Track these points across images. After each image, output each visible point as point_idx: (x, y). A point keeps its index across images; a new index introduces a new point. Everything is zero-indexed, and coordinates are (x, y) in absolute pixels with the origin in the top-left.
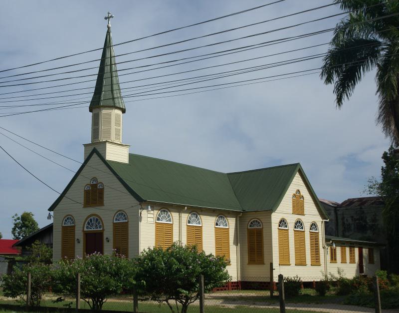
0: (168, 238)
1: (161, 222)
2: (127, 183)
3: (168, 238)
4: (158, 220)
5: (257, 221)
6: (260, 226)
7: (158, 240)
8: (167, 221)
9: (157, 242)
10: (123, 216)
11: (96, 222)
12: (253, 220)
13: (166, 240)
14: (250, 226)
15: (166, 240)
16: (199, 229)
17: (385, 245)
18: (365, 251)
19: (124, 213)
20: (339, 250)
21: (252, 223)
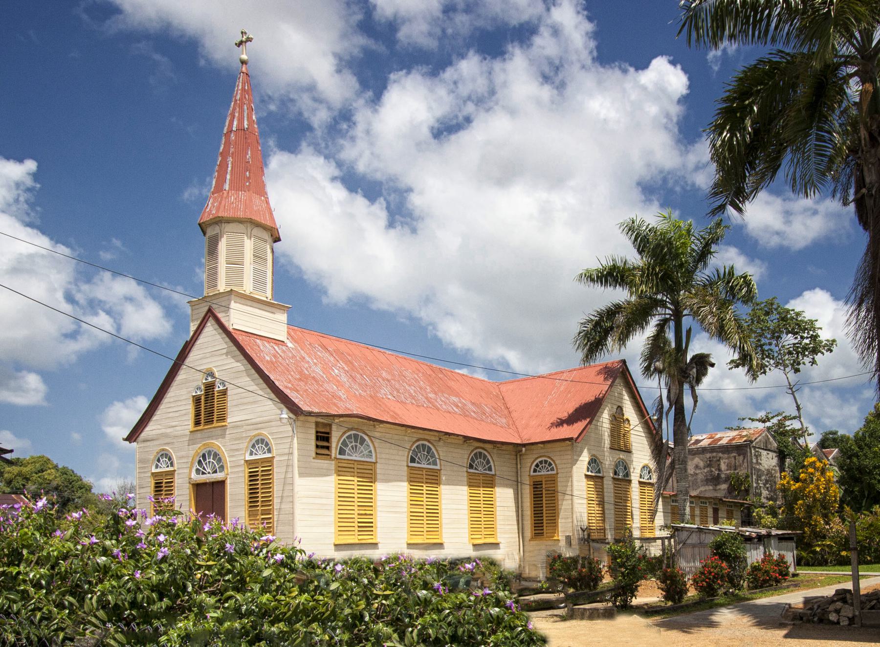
0: (415, 476)
1: (540, 474)
2: (555, 444)
3: (415, 476)
4: (340, 454)
5: (546, 462)
6: (552, 469)
7: (412, 476)
8: (485, 470)
9: (412, 476)
10: (544, 465)
11: (424, 451)
12: (540, 459)
13: (352, 504)
14: (535, 471)
15: (352, 504)
16: (475, 525)
17: (218, 209)
18: (728, 135)
19: (549, 460)
20: (847, 44)
21: (537, 466)
